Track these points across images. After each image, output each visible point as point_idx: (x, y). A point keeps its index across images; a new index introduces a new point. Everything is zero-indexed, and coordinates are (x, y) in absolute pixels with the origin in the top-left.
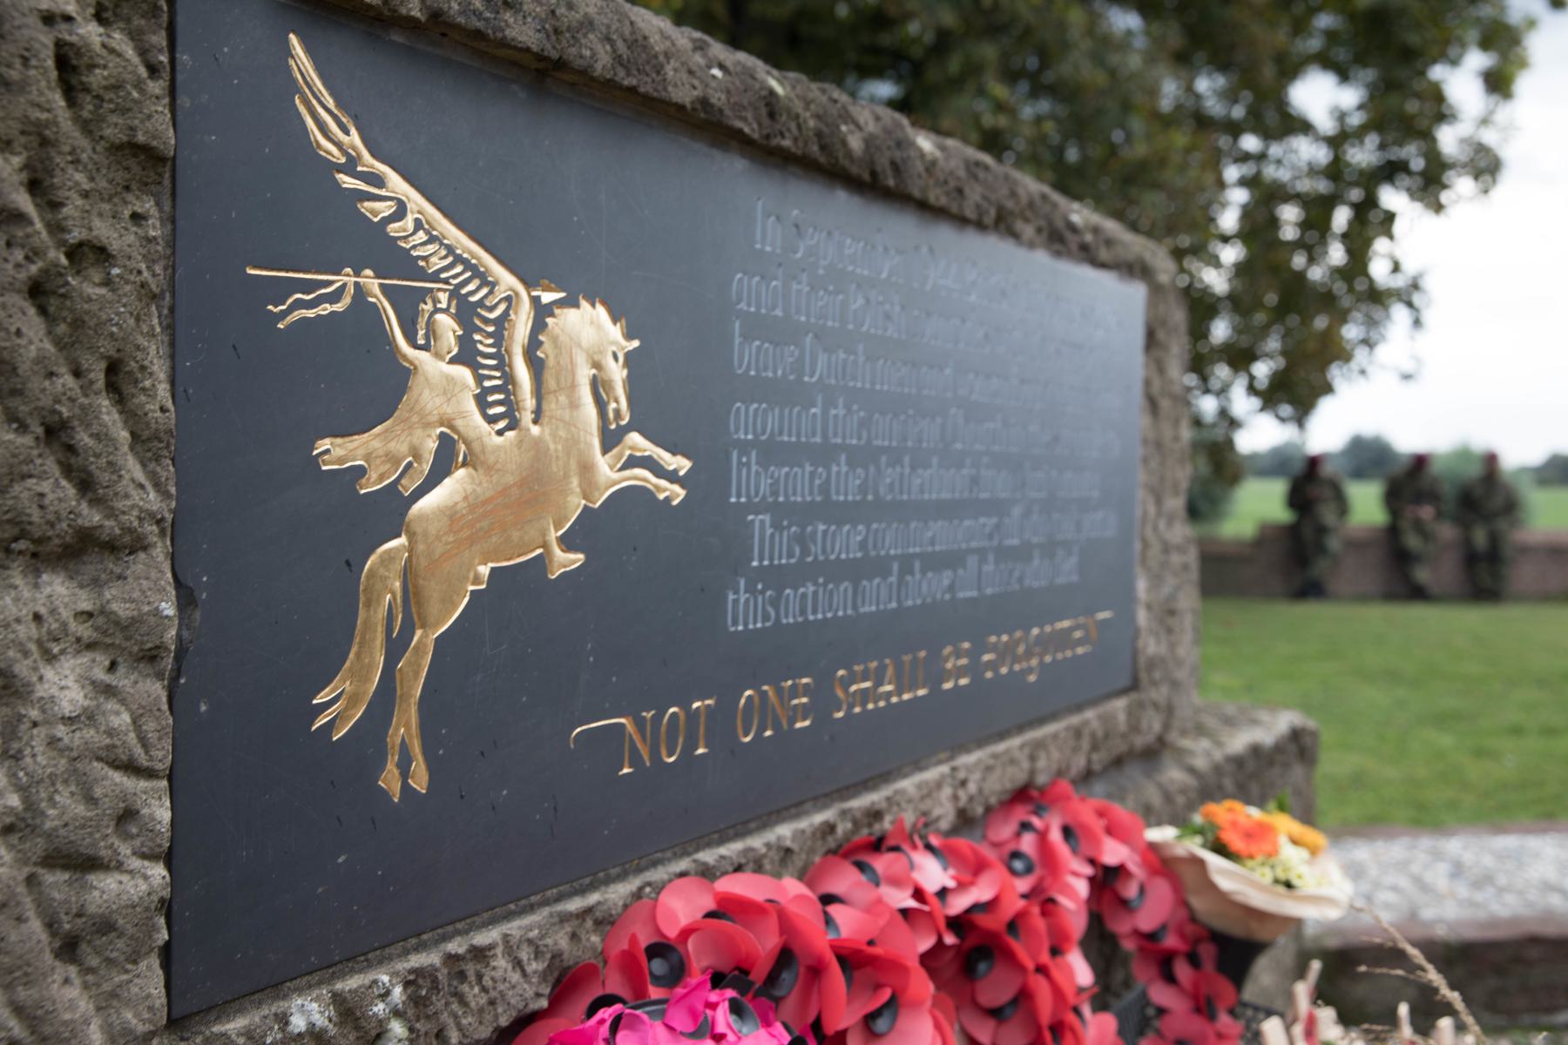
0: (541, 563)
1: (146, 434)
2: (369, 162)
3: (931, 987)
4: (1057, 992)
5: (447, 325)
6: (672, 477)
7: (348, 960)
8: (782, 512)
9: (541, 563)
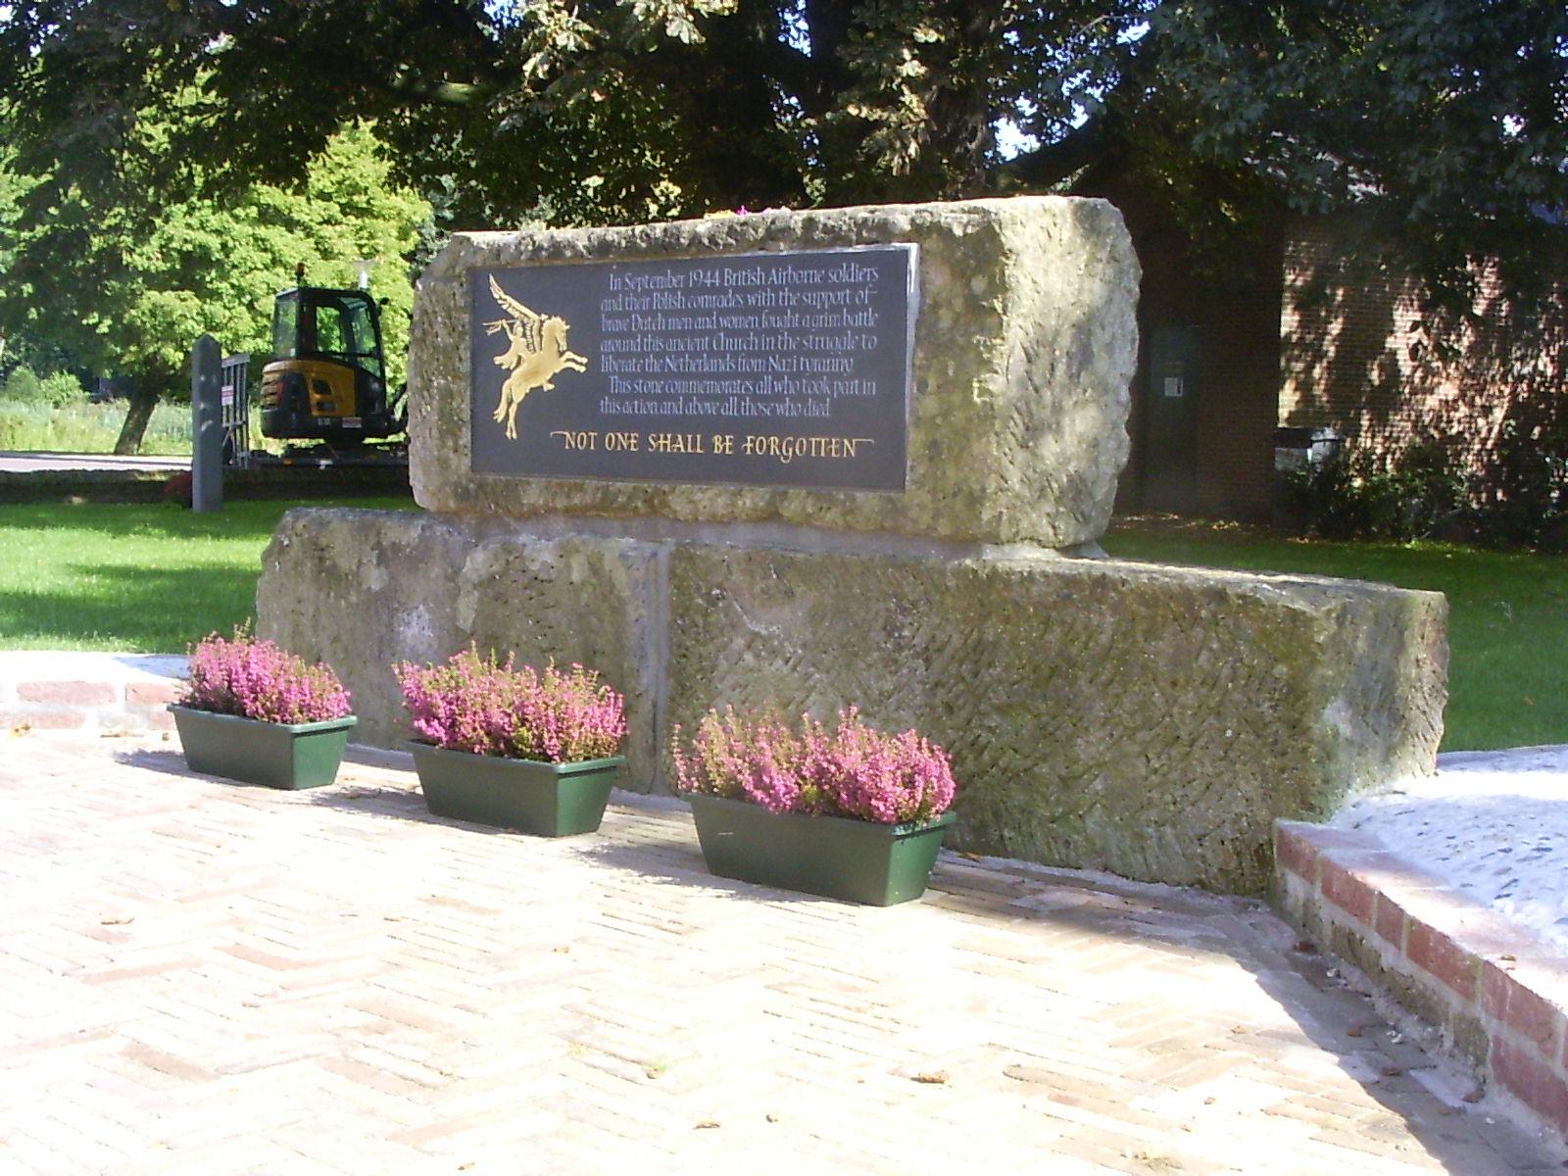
0: (541, 387)
1: (1015, 779)
2: (504, 296)
3: (1450, 1104)
4: (1087, 839)
5: (521, 329)
6: (581, 364)
7: (1123, 876)
8: (623, 376)
9: (541, 387)
